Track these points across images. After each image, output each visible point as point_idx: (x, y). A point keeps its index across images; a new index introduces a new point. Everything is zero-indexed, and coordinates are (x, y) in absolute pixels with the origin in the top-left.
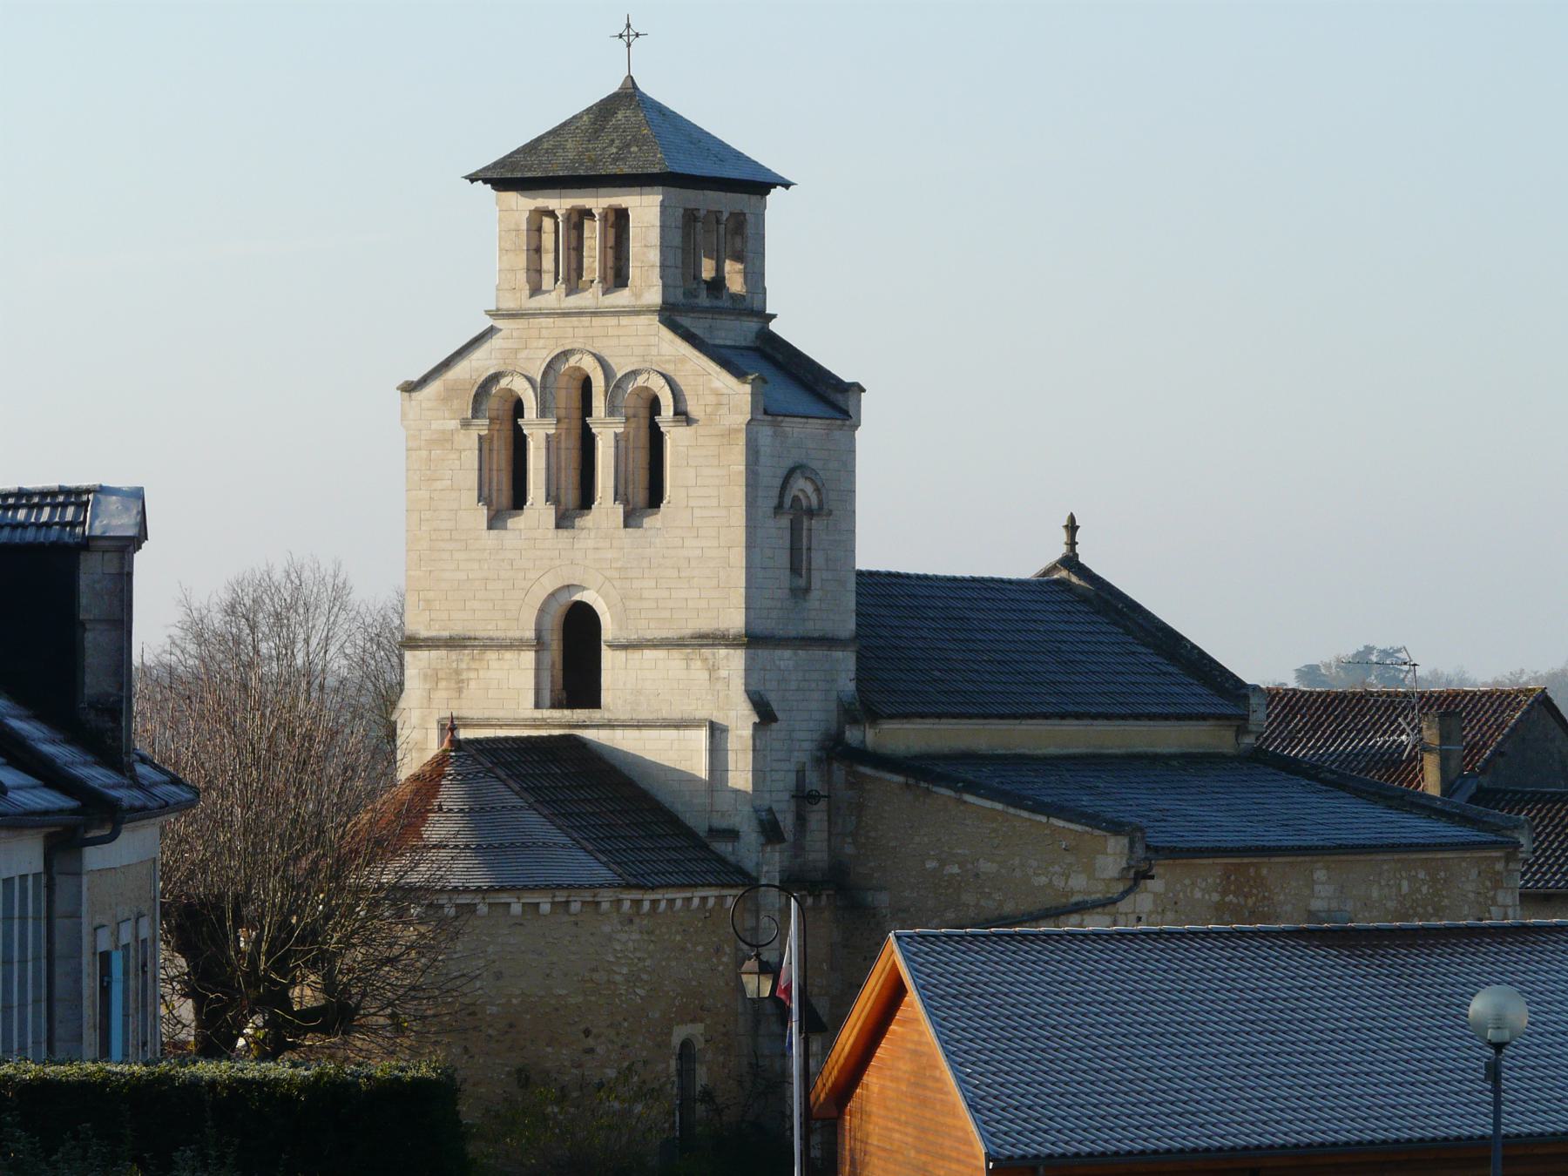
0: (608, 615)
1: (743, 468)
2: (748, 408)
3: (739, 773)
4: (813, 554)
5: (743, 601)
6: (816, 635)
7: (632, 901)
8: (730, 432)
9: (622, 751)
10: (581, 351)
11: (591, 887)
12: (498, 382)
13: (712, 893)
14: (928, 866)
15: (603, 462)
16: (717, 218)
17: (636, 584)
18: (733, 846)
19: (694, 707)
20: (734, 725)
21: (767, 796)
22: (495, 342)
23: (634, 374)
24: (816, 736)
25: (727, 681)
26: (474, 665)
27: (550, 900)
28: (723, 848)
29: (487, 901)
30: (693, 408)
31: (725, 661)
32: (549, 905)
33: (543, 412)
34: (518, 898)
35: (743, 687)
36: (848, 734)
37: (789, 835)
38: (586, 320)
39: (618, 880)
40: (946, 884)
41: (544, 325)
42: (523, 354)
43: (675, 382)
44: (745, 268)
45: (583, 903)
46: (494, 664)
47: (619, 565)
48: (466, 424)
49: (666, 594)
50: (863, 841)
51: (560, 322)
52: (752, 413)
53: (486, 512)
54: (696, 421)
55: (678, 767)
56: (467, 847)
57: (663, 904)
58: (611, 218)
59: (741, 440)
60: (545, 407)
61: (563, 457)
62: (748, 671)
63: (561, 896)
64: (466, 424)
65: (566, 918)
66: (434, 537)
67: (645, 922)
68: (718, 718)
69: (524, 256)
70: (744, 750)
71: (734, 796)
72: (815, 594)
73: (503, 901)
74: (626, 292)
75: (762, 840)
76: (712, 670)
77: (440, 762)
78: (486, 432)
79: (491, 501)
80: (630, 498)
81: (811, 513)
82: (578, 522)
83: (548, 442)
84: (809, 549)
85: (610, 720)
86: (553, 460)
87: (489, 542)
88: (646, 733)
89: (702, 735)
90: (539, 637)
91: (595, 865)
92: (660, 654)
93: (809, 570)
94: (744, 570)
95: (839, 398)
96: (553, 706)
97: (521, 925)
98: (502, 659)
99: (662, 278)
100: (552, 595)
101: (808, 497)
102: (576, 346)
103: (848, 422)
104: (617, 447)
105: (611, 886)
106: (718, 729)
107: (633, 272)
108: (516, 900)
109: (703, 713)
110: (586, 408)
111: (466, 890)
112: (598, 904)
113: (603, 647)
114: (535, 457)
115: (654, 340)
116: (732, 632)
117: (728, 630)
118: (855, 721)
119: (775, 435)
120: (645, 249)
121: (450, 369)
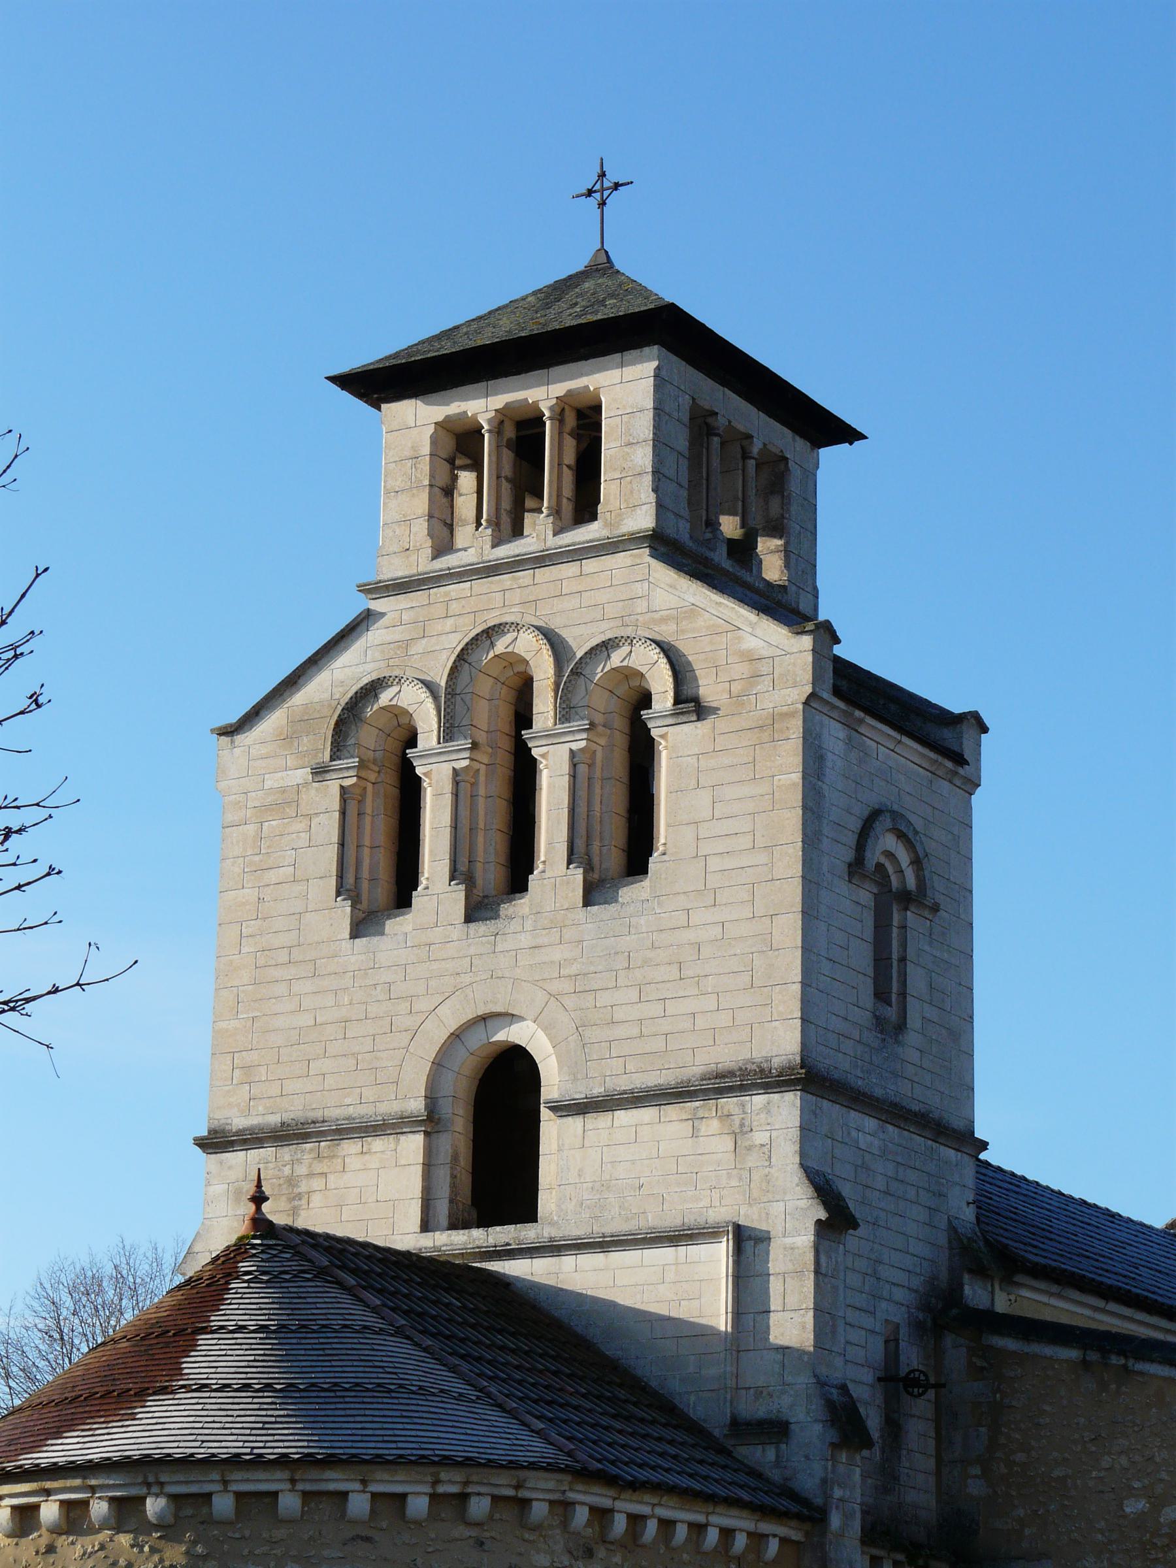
0: (553, 1061)
1: (796, 777)
2: (808, 676)
3: (788, 1315)
4: (910, 968)
5: (798, 1005)
6: (915, 1107)
7: (593, 1509)
8: (775, 719)
9: (572, 1292)
10: (517, 626)
11: (513, 1466)
12: (376, 697)
13: (742, 1523)
14: (1128, 1510)
15: (549, 803)
16: (743, 448)
17: (604, 999)
18: (778, 1450)
19: (705, 1202)
20: (780, 1229)
21: (838, 1362)
22: (374, 636)
23: (607, 646)
24: (916, 1282)
25: (768, 1150)
26: (319, 1167)
27: (428, 1489)
28: (763, 1455)
29: (300, 1486)
30: (708, 689)
31: (763, 1116)
32: (427, 1499)
33: (448, 732)
34: (364, 1482)
35: (797, 1160)
36: (967, 1290)
37: (873, 1421)
38: (525, 577)
39: (564, 1461)
40: (1166, 1541)
41: (453, 595)
42: (419, 647)
43: (677, 650)
44: (786, 544)
45: (496, 1499)
46: (354, 1163)
47: (574, 969)
48: (320, 772)
49: (657, 1009)
50: (1004, 1471)
51: (481, 585)
52: (814, 683)
53: (348, 909)
54: (714, 710)
55: (674, 1314)
56: (268, 1387)
57: (652, 1527)
58: (571, 421)
59: (795, 729)
60: (452, 726)
61: (481, 812)
62: (806, 1130)
63: (451, 1482)
64: (320, 772)
65: (461, 1531)
66: (261, 962)
67: (617, 1559)
68: (750, 1218)
69: (425, 496)
70: (799, 1273)
71: (780, 1357)
72: (912, 1038)
73: (332, 1487)
74: (595, 526)
75: (832, 1435)
76: (739, 1133)
77: (238, 1250)
78: (354, 780)
79: (358, 895)
80: (596, 860)
81: (906, 899)
82: (506, 909)
83: (456, 783)
84: (903, 960)
85: (551, 1240)
86: (464, 812)
87: (353, 959)
88: (618, 1258)
89: (721, 1252)
90: (432, 1101)
91: (524, 1434)
92: (646, 1114)
93: (903, 994)
94: (799, 953)
95: (947, 735)
96: (453, 1226)
97: (368, 1539)
98: (369, 1152)
99: (655, 490)
100: (456, 1036)
101: (901, 871)
102: (508, 619)
103: (961, 771)
104: (573, 776)
105: (551, 1468)
106: (750, 1238)
107: (608, 489)
108: (357, 1486)
109: (721, 1212)
110: (523, 718)
111: (259, 1462)
112: (525, 1503)
113: (545, 1113)
114: (432, 811)
115: (640, 589)
116: (776, 1062)
117: (768, 1060)
118: (980, 1272)
119: (849, 742)
120: (626, 449)
121: (299, 690)
